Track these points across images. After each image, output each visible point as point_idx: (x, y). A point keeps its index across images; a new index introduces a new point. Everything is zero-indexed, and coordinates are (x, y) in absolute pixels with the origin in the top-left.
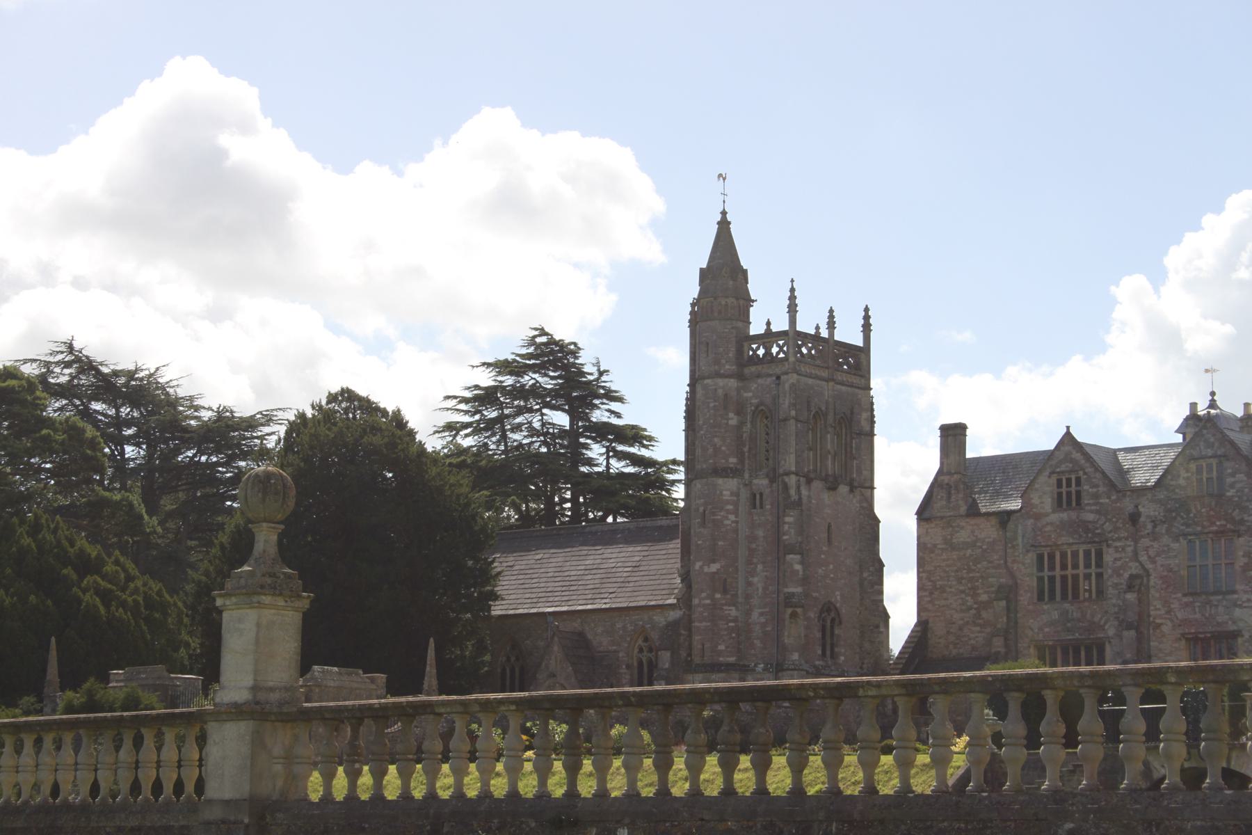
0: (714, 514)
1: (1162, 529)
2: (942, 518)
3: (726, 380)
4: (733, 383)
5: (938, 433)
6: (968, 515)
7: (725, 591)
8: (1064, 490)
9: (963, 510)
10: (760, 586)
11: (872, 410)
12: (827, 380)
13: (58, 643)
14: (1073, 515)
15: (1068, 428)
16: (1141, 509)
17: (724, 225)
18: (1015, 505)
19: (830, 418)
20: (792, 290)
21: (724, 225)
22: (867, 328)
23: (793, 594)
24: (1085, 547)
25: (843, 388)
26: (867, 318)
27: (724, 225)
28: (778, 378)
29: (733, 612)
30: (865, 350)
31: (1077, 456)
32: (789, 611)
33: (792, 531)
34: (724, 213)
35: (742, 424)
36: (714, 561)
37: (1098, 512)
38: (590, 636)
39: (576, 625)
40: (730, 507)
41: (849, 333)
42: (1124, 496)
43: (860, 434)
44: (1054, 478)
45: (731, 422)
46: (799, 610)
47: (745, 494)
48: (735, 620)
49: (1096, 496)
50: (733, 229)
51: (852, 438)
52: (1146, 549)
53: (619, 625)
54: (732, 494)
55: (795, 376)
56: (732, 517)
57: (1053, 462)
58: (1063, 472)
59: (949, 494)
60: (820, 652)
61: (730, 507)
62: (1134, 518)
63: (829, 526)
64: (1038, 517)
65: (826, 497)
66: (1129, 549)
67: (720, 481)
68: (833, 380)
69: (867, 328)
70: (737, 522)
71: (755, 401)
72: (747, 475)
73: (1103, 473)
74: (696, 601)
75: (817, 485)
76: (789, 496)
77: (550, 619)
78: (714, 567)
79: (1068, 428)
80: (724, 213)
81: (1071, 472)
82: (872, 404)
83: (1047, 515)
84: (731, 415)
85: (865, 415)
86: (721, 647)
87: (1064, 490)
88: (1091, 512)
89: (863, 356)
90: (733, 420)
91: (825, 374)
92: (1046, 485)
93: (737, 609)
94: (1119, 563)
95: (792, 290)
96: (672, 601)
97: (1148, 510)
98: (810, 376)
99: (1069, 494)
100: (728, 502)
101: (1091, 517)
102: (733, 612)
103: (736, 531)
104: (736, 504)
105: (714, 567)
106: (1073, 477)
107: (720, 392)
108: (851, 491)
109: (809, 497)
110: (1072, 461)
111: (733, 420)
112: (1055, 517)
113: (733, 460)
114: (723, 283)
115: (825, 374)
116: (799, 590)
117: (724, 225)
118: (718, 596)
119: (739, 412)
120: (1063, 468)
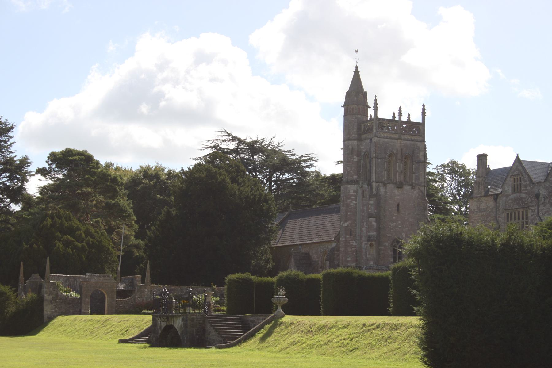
0: (346, 201)
1: (547, 201)
2: (476, 197)
3: (353, 141)
4: (355, 143)
5: (476, 158)
6: (485, 196)
7: (351, 235)
8: (516, 183)
9: (483, 193)
10: (365, 232)
11: (425, 151)
12: (397, 139)
13: (23, 265)
14: (518, 194)
15: (518, 154)
16: (540, 192)
17: (357, 72)
18: (499, 191)
19: (399, 156)
20: (376, 100)
21: (357, 72)
22: (424, 114)
23: (372, 235)
24: (522, 210)
25: (408, 142)
26: (424, 109)
27: (357, 73)
28: (371, 140)
29: (354, 244)
30: (423, 124)
31: (520, 167)
32: (369, 243)
33: (373, 208)
34: (357, 67)
35: (360, 161)
36: (346, 221)
37: (526, 193)
38: (311, 254)
39: (304, 250)
40: (353, 197)
41: (416, 118)
42: (535, 186)
43: (419, 162)
44: (513, 178)
45: (354, 160)
46: (373, 243)
47: (360, 191)
48: (355, 247)
49: (526, 186)
50: (361, 74)
51: (413, 164)
52: (542, 210)
53: (319, 250)
54: (354, 192)
55: (376, 138)
56: (354, 202)
57: (512, 171)
58: (515, 175)
59: (479, 186)
60: (392, 260)
61: (353, 197)
62: (537, 196)
63: (398, 205)
64: (507, 196)
65: (396, 191)
66: (536, 210)
67: (349, 186)
68: (400, 139)
69: (424, 114)
70: (356, 204)
71: (364, 150)
72: (361, 183)
73: (528, 175)
74: (341, 239)
75: (390, 186)
76: (372, 192)
77: (300, 247)
78: (346, 224)
79: (518, 154)
80: (357, 67)
81: (518, 175)
82: (425, 148)
83: (510, 195)
84: (355, 157)
85: (421, 153)
86: (349, 259)
87: (516, 183)
88: (524, 193)
89: (421, 127)
90: (356, 159)
91: (397, 136)
92: (510, 180)
93: (356, 242)
94: (533, 217)
95: (376, 100)
96: (333, 239)
97: (543, 192)
98: (387, 138)
99: (517, 184)
100: (352, 195)
101: (524, 196)
102: (354, 244)
103: (356, 208)
104: (356, 196)
105: (346, 224)
106: (516, 178)
107: (350, 147)
108: (412, 188)
109: (386, 192)
110: (519, 170)
111: (356, 159)
112: (512, 196)
113: (355, 177)
114: (356, 98)
115: (397, 136)
116: (375, 233)
117: (357, 73)
118: (348, 237)
119: (358, 155)
120: (515, 173)
